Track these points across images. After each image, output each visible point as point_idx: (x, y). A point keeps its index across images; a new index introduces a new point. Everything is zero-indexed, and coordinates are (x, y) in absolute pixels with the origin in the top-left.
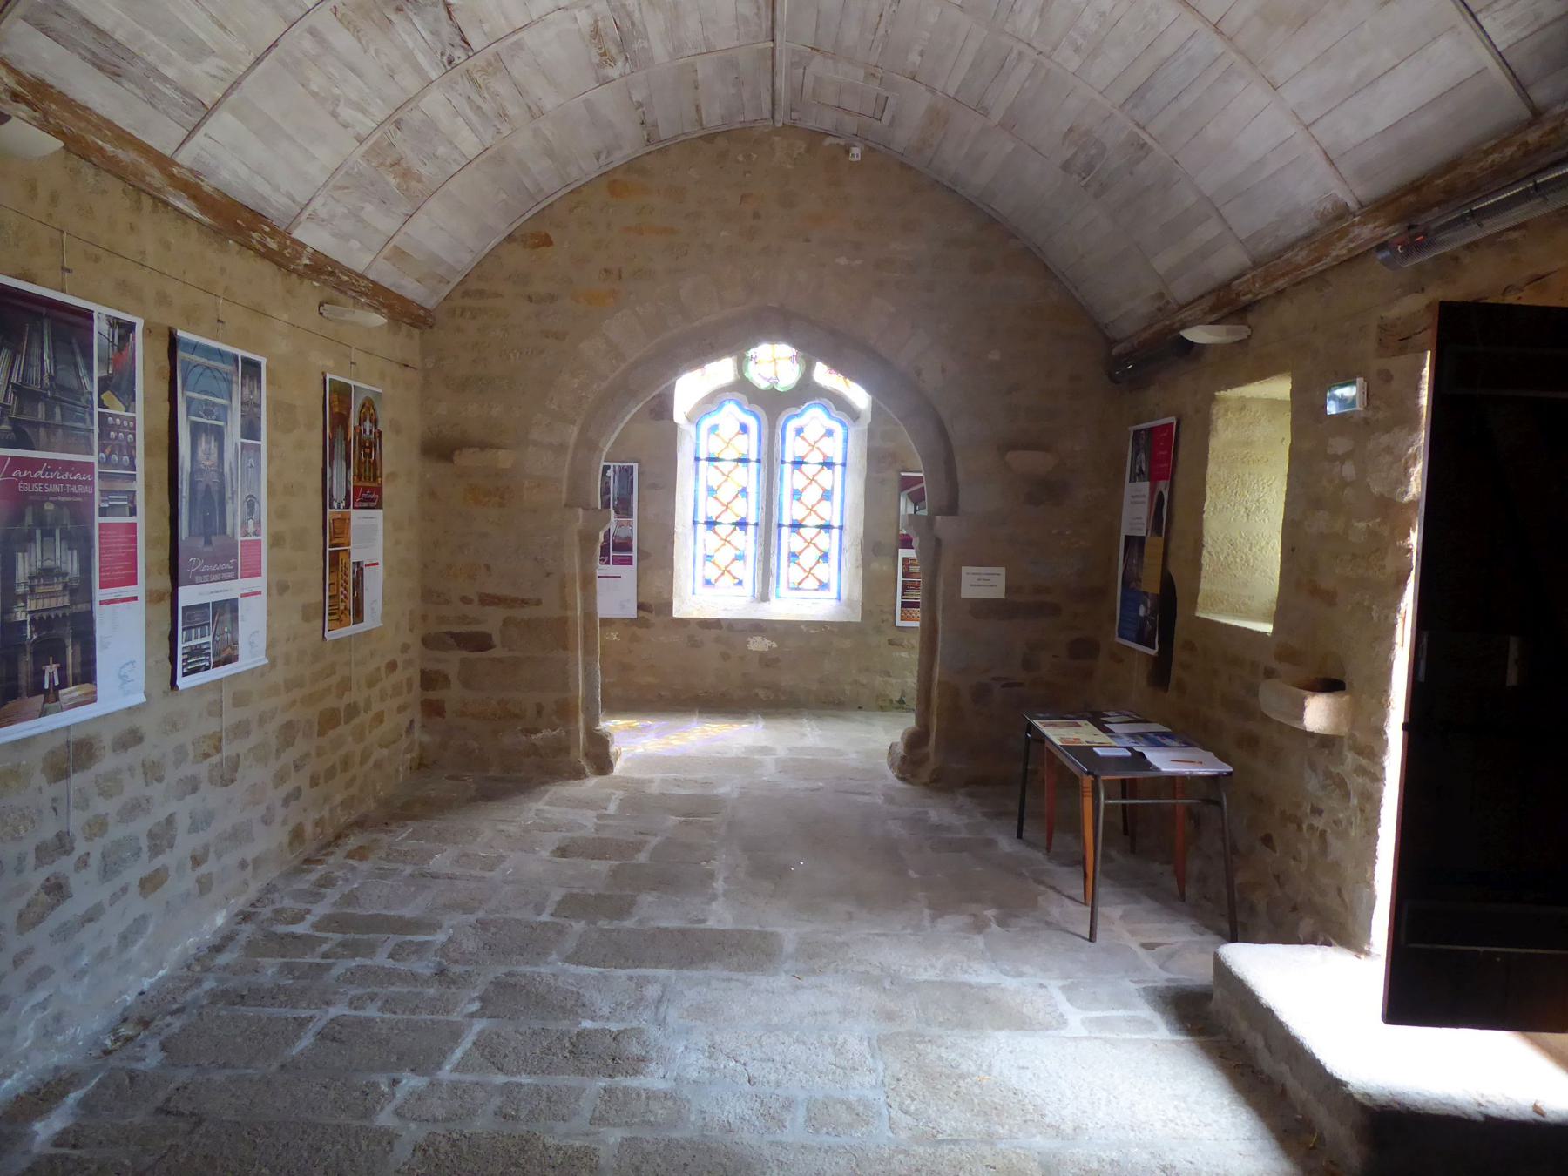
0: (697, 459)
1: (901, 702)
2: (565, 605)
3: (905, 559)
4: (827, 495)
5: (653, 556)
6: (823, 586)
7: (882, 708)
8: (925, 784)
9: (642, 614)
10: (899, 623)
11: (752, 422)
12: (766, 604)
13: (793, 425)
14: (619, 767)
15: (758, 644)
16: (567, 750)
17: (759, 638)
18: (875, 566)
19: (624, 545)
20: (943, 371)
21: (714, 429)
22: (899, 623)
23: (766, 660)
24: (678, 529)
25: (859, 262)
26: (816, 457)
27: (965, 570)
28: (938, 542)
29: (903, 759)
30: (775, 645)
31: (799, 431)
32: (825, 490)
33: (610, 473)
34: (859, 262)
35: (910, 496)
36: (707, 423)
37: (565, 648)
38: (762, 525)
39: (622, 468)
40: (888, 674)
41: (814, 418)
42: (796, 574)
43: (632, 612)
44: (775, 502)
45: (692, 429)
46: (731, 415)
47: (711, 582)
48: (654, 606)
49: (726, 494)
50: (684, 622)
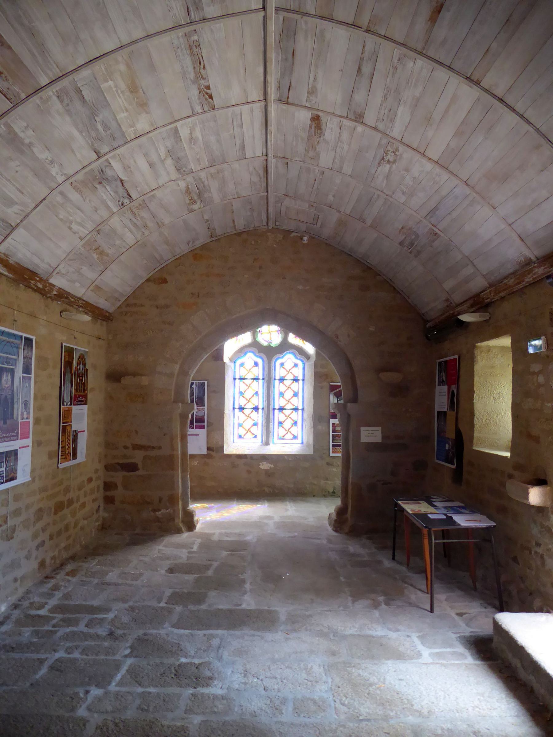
0: (235, 379)
1: (334, 492)
3: (333, 424)
4: (296, 394)
5: (214, 424)
6: (295, 437)
7: (325, 496)
11: (260, 361)
12: (268, 447)
15: (265, 466)
16: (174, 520)
17: (265, 463)
18: (320, 427)
19: (200, 420)
20: (349, 336)
21: (242, 365)
22: (331, 455)
23: (269, 474)
24: (226, 411)
25: (308, 288)
29: (336, 521)
31: (282, 365)
33: (194, 386)
36: (239, 362)
37: (173, 470)
39: (199, 384)
41: (289, 359)
42: (282, 432)
43: (205, 452)
46: (250, 358)
47: (242, 437)
48: (215, 448)
50: (229, 456)
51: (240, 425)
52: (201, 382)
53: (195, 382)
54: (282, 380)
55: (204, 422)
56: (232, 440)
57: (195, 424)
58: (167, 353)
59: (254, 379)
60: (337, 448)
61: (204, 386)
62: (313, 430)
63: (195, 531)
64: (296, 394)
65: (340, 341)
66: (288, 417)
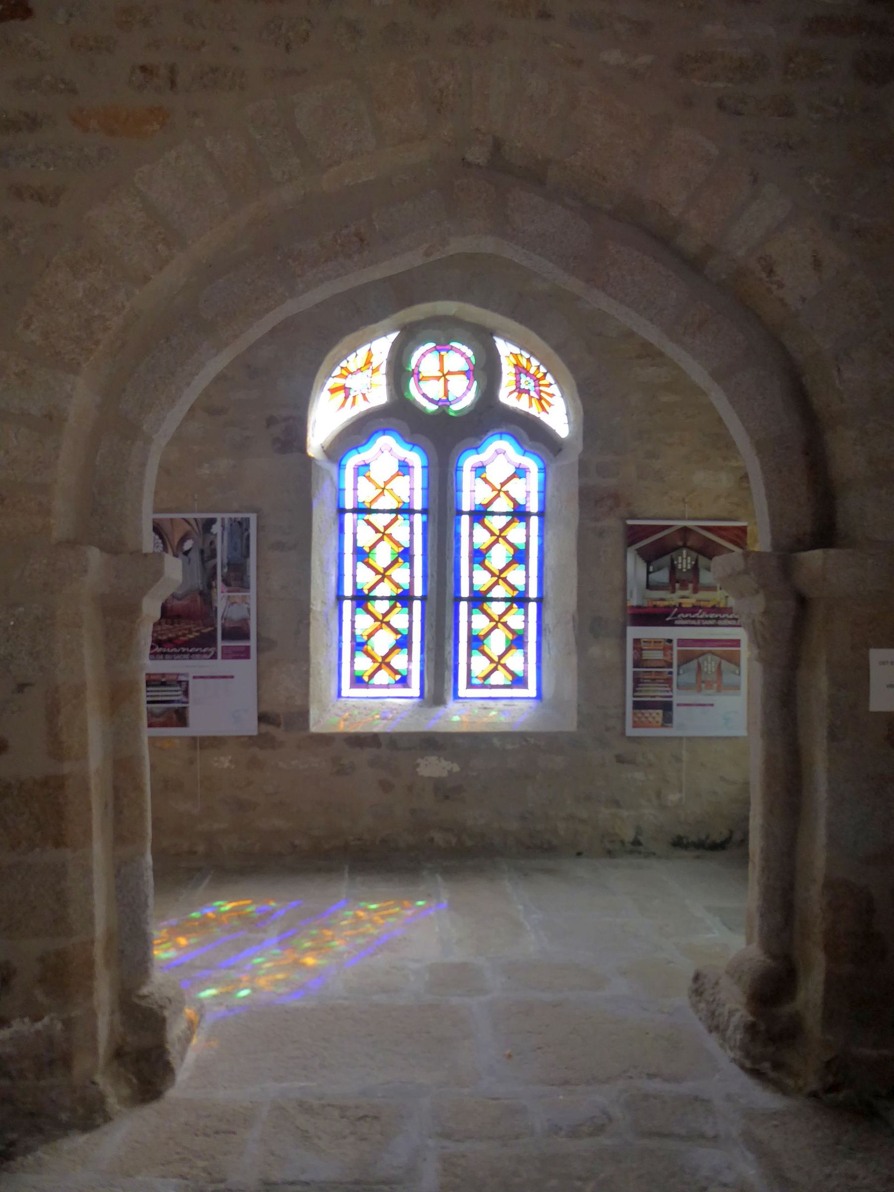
0: (342, 511)
1: (636, 843)
2: (57, 749)
3: (637, 641)
4: (520, 557)
5: (285, 644)
6: (519, 681)
7: (610, 853)
8: (814, 1095)
9: (266, 728)
10: (630, 731)
11: (416, 459)
12: (440, 710)
13: (469, 461)
14: (192, 1056)
15: (433, 767)
16: (66, 1061)
17: (433, 759)
18: (595, 651)
19: (238, 632)
20: (817, 264)
21: (362, 469)
22: (630, 731)
23: (445, 791)
24: (317, 606)
25: (645, 59)
26: (503, 505)
27: (876, 655)
28: (802, 602)
29: (751, 1029)
30: (456, 768)
31: (480, 469)
32: (482, 564)
33: (216, 529)
34: (645, 59)
35: (641, 553)
36: (352, 460)
37: (59, 843)
38: (432, 599)
39: (233, 521)
40: (617, 804)
41: (500, 455)
42: (480, 665)
43: (251, 727)
44: (450, 565)
45: (334, 469)
46: (386, 452)
47: (365, 679)
48: (283, 719)
49: (383, 555)
50: (326, 739)
51: (359, 646)
52: (239, 516)
53: (218, 516)
54: (479, 515)
55: (247, 637)
56: (334, 691)
57: (220, 643)
58: (27, 326)
59: (398, 511)
60: (647, 712)
61: (247, 529)
62: (574, 659)
63: (172, 1093)
64: (520, 557)
65: (781, 286)
66: (498, 622)
